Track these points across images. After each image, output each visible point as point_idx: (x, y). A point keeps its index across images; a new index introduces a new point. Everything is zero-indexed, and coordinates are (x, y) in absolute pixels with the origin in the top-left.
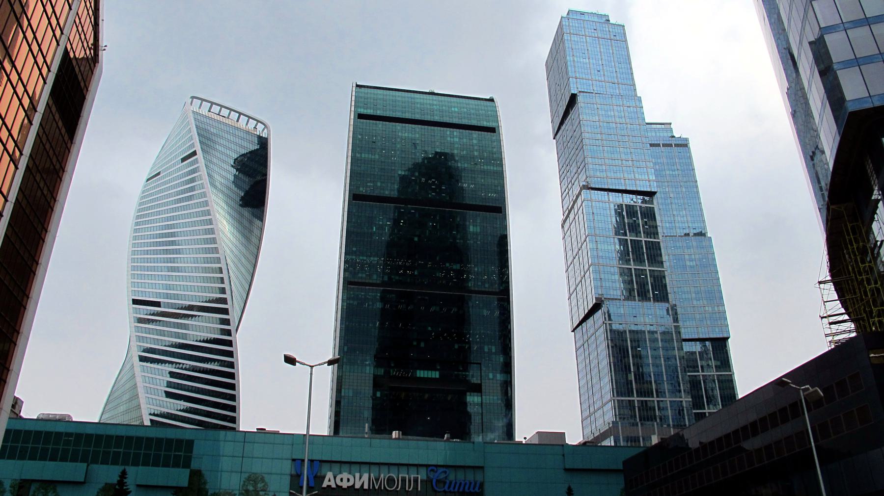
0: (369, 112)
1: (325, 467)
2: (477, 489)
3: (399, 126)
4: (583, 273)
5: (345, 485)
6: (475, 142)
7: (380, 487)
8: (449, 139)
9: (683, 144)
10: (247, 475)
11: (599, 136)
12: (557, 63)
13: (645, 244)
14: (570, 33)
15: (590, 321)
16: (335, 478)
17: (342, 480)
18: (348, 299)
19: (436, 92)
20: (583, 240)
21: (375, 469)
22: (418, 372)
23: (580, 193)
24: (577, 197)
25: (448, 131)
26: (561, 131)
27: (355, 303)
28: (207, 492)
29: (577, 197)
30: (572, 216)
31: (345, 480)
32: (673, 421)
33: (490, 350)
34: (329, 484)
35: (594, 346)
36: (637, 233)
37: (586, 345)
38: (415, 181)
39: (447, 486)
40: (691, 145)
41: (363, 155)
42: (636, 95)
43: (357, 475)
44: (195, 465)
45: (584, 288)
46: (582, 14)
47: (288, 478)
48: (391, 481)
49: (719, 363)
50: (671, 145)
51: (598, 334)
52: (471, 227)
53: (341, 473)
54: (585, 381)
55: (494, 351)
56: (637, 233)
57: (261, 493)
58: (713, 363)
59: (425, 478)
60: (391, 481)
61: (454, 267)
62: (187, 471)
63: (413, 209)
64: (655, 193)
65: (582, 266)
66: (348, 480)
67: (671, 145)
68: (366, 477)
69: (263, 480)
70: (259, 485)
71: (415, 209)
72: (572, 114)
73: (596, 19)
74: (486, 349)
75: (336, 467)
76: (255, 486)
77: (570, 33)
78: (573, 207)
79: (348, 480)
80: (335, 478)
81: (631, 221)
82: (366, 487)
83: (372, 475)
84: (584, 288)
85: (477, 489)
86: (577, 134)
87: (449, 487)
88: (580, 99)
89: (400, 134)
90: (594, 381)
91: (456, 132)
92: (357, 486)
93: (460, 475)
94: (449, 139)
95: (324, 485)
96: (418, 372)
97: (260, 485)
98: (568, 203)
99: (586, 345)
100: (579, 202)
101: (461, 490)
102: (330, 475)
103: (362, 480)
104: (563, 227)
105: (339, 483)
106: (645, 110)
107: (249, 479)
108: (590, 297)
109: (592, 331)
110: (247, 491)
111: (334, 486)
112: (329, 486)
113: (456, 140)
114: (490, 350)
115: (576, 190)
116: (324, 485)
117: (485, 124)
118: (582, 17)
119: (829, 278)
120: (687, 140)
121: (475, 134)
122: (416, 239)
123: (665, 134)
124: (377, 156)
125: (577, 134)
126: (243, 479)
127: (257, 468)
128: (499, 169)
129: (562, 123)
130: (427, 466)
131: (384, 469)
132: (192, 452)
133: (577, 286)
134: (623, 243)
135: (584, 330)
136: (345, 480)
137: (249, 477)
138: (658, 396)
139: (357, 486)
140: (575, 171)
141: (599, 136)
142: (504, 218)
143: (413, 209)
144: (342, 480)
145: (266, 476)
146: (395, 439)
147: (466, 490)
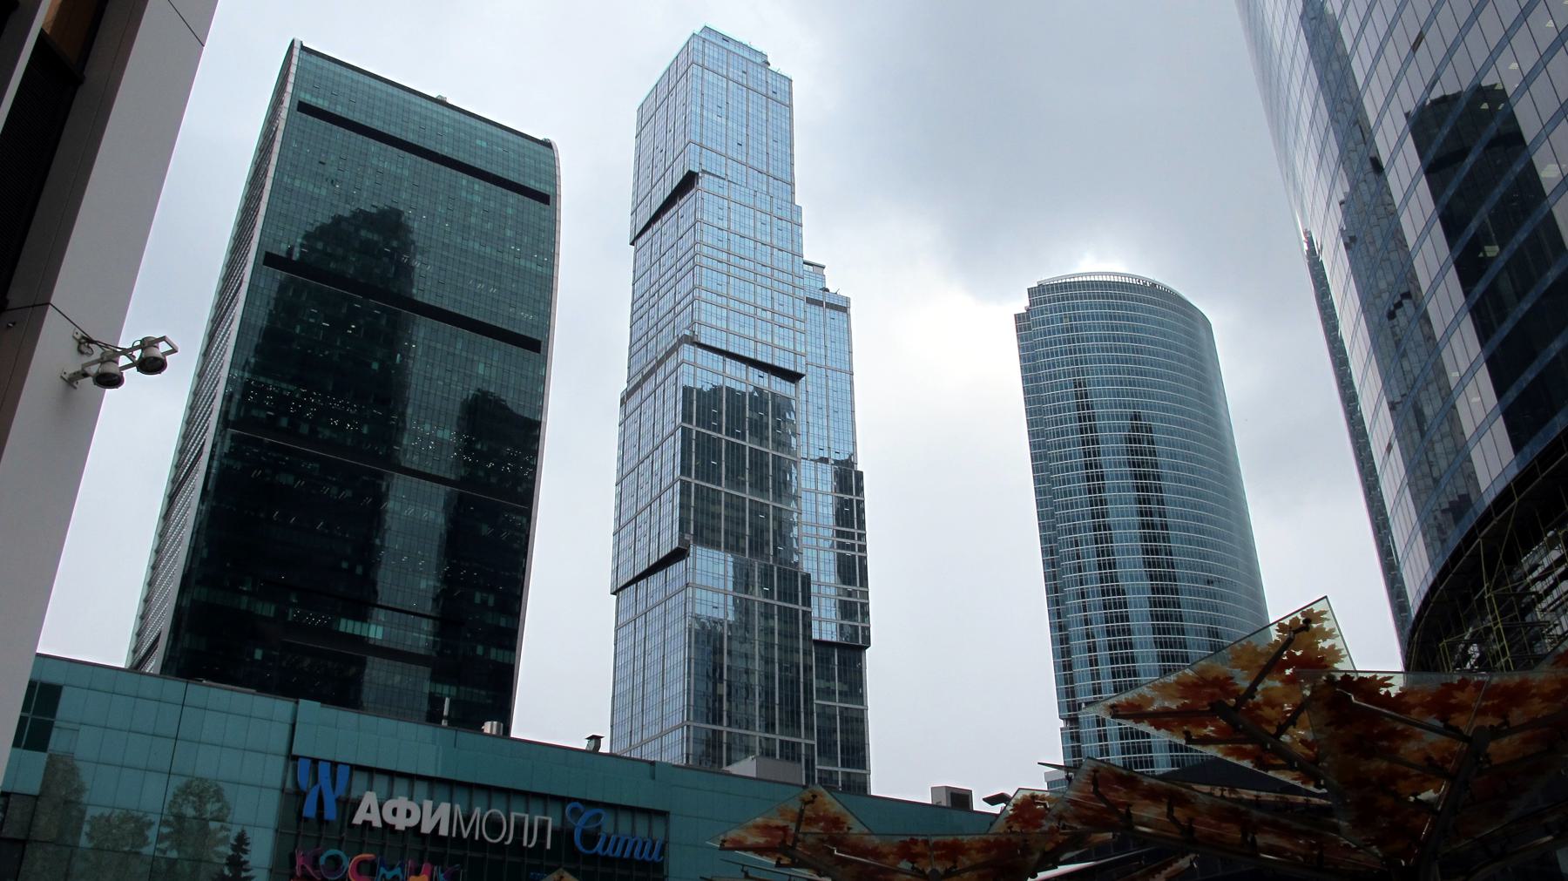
0: (321, 103)
1: (360, 780)
2: (655, 856)
3: (375, 146)
4: (656, 492)
5: (401, 823)
6: (510, 211)
7: (472, 834)
8: (464, 194)
9: (841, 308)
10: (185, 780)
11: (724, 256)
12: (662, 107)
13: (745, 466)
14: (702, 66)
15: (657, 580)
16: (381, 808)
17: (394, 812)
18: (233, 454)
19: (450, 101)
20: (667, 431)
21: (461, 795)
22: (343, 621)
23: (674, 349)
24: (668, 354)
25: (464, 179)
26: (649, 232)
27: (238, 465)
28: (83, 813)
29: (668, 354)
30: (648, 386)
31: (402, 813)
32: (1243, 755)
33: (484, 602)
34: (368, 817)
35: (658, 625)
36: (762, 440)
37: (640, 622)
38: (390, 256)
39: (600, 845)
40: (852, 311)
41: (297, 183)
42: (793, 202)
43: (428, 805)
44: (57, 742)
45: (655, 519)
46: (726, 39)
47: (276, 795)
48: (494, 826)
49: (846, 688)
50: (819, 303)
51: (670, 604)
52: (481, 366)
53: (390, 797)
54: (628, 685)
55: (491, 602)
56: (762, 440)
57: (213, 825)
58: (837, 686)
59: (558, 824)
60: (494, 826)
61: (440, 434)
62: (42, 758)
63: (378, 307)
64: (800, 376)
65: (656, 480)
66: (409, 814)
67: (819, 303)
68: (445, 808)
69: (218, 795)
70: (209, 807)
71: (383, 310)
72: (686, 204)
73: (746, 55)
74: (478, 598)
75: (381, 782)
76: (199, 808)
77: (702, 66)
78: (653, 371)
79: (409, 814)
80: (381, 808)
81: (755, 416)
82: (443, 831)
83: (457, 807)
84: (655, 519)
85: (655, 856)
86: (688, 241)
87: (605, 848)
88: (704, 182)
89: (375, 161)
90: (649, 688)
91: (479, 185)
92: (426, 828)
93: (625, 824)
94: (464, 194)
95: (358, 820)
96: (343, 621)
97: (211, 807)
98: (642, 361)
99: (640, 622)
100: (671, 364)
101: (626, 855)
102: (370, 799)
103: (435, 816)
104: (623, 402)
105: (389, 819)
106: (805, 231)
107: (186, 791)
108: (666, 536)
109: (659, 596)
110: (180, 818)
111: (377, 823)
112: (367, 824)
113: (477, 199)
114: (484, 602)
115: (667, 340)
116: (358, 820)
117: (532, 184)
118: (725, 44)
119: (428, 608)
120: (847, 300)
121: (513, 198)
122: (375, 366)
123: (813, 283)
124: (324, 192)
125: (688, 241)
126: (171, 791)
127: (207, 765)
128: (545, 270)
129: (655, 218)
130: (564, 800)
131: (481, 798)
132: (53, 715)
133: (638, 513)
134: (782, 444)
135: (642, 593)
136: (402, 813)
137: (188, 786)
138: (729, 725)
139: (426, 828)
140: (667, 308)
141: (724, 256)
142: (544, 362)
143: (378, 307)
144: (394, 812)
145: (226, 787)
146: (490, 735)
147: (636, 855)
